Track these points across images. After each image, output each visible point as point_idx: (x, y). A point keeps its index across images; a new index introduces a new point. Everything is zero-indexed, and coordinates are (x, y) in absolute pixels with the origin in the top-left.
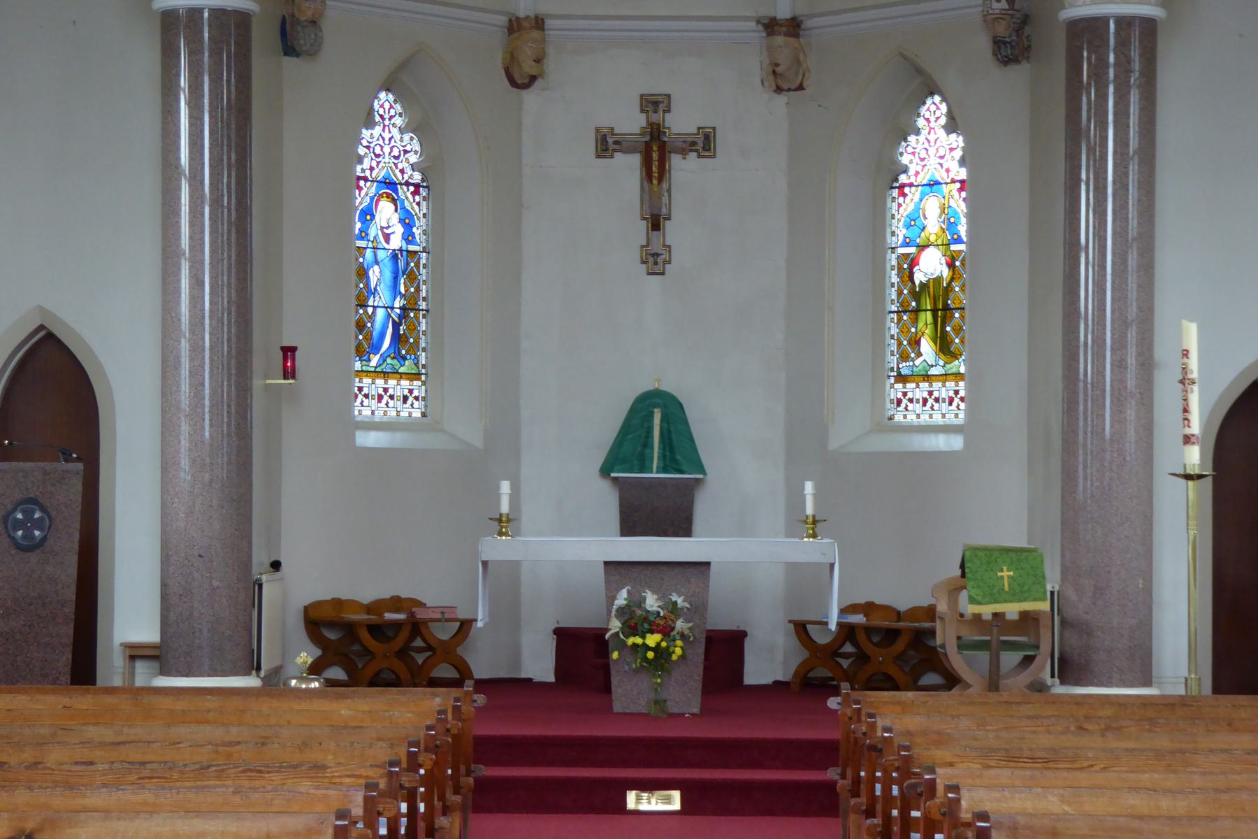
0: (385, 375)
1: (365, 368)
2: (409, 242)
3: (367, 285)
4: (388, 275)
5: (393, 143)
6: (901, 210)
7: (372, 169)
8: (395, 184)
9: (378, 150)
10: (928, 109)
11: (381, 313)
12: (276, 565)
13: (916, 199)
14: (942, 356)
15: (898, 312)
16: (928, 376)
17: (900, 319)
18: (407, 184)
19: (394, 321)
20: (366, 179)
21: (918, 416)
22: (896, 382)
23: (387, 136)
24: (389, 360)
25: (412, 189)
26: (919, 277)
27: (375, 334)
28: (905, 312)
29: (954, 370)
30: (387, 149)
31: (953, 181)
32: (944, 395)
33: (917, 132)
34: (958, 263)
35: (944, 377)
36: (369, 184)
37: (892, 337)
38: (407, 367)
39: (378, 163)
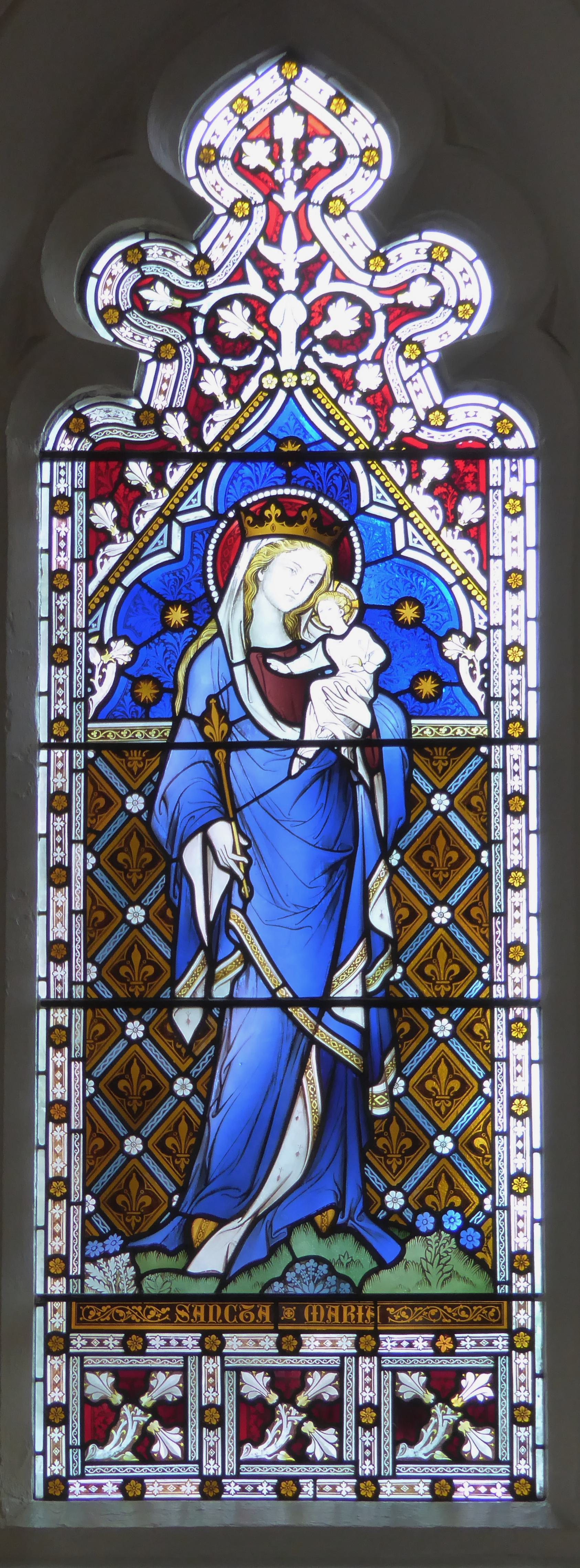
0: (284, 1313)
1: (153, 1285)
2: (411, 703)
3: (173, 908)
4: (296, 860)
5: (324, 284)
7: (199, 407)
8: (339, 456)
9: (236, 323)
11: (250, 1036)
12: (297, 1154)
17: (96, 1043)
18: (411, 452)
19: (331, 1064)
20: (162, 454)
23: (288, 256)
24: (305, 1243)
25: (436, 469)
27: (221, 1128)
30: (288, 315)
36: (175, 475)
38: (423, 1265)
39: (236, 382)
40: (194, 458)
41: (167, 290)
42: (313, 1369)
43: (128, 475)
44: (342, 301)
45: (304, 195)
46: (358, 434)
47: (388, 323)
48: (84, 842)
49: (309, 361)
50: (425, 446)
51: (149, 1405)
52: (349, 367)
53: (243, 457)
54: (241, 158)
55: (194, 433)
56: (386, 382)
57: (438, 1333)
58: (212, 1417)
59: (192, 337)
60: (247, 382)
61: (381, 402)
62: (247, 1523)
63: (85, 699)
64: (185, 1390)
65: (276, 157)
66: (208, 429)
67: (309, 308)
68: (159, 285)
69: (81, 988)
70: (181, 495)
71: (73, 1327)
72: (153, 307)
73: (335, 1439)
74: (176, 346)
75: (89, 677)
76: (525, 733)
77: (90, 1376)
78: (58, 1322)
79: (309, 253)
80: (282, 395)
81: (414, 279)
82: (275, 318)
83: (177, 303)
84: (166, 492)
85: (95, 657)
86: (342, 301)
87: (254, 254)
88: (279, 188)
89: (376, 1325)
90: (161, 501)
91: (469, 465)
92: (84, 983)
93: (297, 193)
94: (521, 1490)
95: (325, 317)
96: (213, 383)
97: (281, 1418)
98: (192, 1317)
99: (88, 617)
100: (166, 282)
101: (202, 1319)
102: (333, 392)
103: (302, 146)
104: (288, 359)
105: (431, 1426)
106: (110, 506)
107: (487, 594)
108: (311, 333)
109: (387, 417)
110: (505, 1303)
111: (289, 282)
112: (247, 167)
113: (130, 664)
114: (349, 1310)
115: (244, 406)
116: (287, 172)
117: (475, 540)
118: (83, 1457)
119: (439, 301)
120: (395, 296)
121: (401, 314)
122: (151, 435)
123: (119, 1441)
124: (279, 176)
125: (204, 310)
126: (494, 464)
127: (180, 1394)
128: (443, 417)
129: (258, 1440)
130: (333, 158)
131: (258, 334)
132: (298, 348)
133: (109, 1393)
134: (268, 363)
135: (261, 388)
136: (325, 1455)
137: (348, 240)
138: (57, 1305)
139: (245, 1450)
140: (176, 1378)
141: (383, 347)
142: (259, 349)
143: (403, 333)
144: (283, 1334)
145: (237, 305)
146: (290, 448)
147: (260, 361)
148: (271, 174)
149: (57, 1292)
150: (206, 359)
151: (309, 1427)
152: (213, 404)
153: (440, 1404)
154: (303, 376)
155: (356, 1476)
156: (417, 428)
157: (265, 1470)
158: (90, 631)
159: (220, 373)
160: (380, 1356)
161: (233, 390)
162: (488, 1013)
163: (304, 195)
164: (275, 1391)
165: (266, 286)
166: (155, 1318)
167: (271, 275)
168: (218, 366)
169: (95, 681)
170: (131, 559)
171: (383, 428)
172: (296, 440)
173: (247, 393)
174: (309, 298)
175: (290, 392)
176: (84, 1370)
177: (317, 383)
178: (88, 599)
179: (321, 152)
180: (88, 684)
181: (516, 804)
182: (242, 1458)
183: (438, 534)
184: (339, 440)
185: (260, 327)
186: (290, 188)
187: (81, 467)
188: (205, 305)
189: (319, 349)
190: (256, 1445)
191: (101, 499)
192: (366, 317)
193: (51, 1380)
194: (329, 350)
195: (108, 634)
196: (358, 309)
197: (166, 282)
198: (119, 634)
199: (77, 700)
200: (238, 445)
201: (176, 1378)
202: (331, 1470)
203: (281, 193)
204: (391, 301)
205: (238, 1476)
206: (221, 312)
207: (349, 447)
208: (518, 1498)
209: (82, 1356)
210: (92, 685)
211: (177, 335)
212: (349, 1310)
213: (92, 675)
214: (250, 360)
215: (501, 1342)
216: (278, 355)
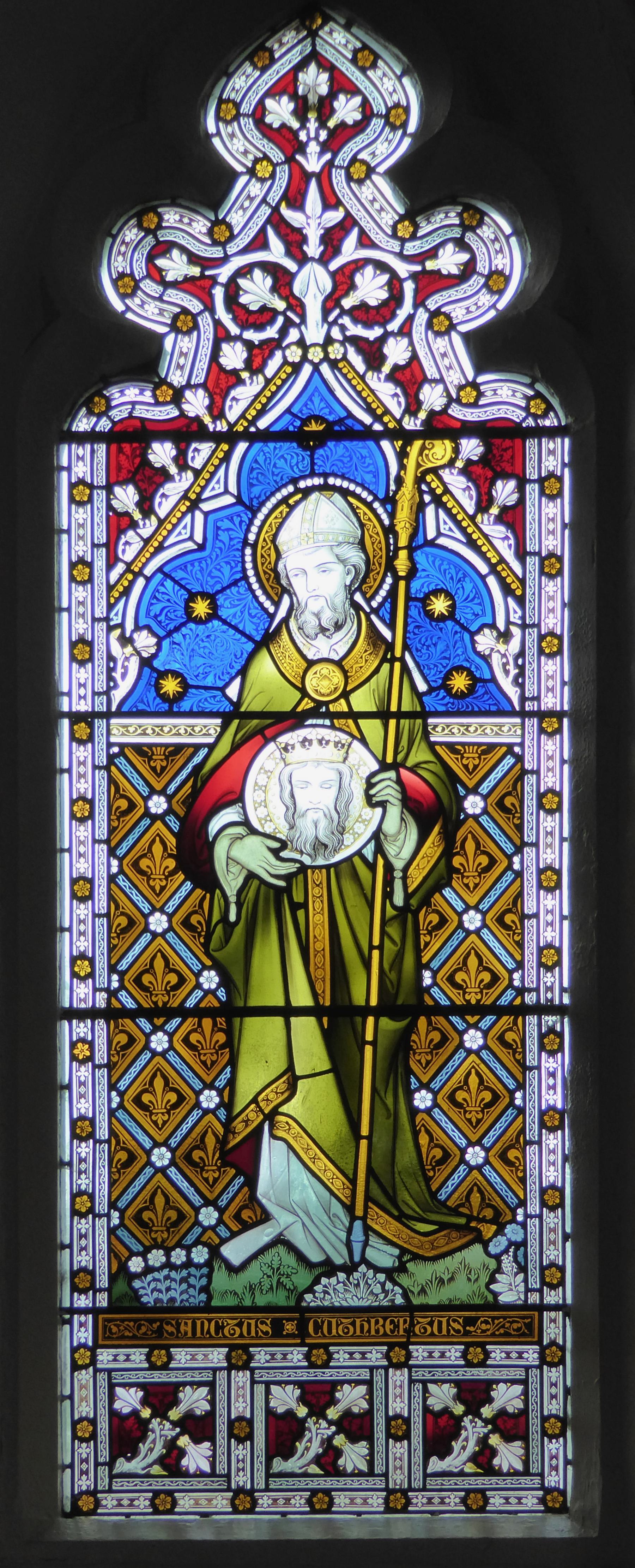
5: (349, 251)
6: (130, 546)
7: (221, 382)
9: (257, 291)
10: (286, 86)
13: (219, 497)
14: (381, 1221)
15: (111, 1014)
16: (302, 1313)
17: (122, 1052)
21: (244, 1499)
22: (105, 1337)
23: (312, 219)
25: (471, 448)
26: (239, 857)
28: (159, 1014)
29: (461, 1290)
30: (313, 283)
31: (439, 427)
32: (240, 1398)
33: (209, 185)
34: (473, 804)
35: (400, 1326)
37: (83, 1130)
39: (256, 357)
40: (217, 438)
41: (185, 258)
42: (498, 1382)
43: (151, 457)
44: (369, 270)
45: (328, 156)
46: (387, 412)
47: (417, 291)
48: (107, 842)
49: (336, 333)
50: (458, 425)
51: (336, 1417)
52: (377, 339)
53: (266, 436)
54: (263, 115)
55: (217, 411)
56: (414, 357)
57: (152, 1348)
58: (399, 1428)
59: (210, 307)
60: (271, 355)
61: (410, 378)
62: (283, 1538)
63: (107, 693)
64: (371, 1402)
65: (301, 113)
66: (231, 407)
67: (333, 275)
68: (175, 253)
69: (104, 995)
70: (207, 476)
71: (100, 1342)
72: (170, 278)
73: (522, 1451)
74: (194, 317)
75: (110, 671)
76: (72, 725)
77: (119, 1391)
78: (85, 1335)
79: (335, 217)
80: (307, 369)
81: (443, 244)
82: (297, 288)
83: (196, 271)
84: (190, 475)
85: (116, 649)
86: (369, 270)
87: (276, 220)
88: (301, 148)
89: (408, 1338)
90: (185, 485)
91: (503, 445)
92: (107, 990)
93: (322, 153)
94: (553, 1502)
95: (352, 287)
96: (233, 357)
97: (310, 1431)
98: (178, 1331)
99: (110, 607)
100: (183, 249)
101: (190, 1334)
102: (361, 367)
103: (327, 102)
104: (314, 332)
105: (305, 1439)
106: (131, 489)
107: (523, 581)
108: (337, 304)
109: (417, 395)
110: (536, 1313)
111: (313, 248)
112: (270, 126)
113: (154, 656)
114: (377, 1322)
115: (268, 381)
116: (311, 131)
117: (510, 525)
118: (110, 1471)
119: (468, 270)
120: (422, 263)
121: (430, 283)
122: (172, 412)
123: (303, 1455)
124: (303, 136)
125: (223, 279)
126: (531, 445)
127: (521, 1406)
128: (474, 393)
129: (288, 1453)
130: (358, 117)
131: (280, 305)
132: (325, 319)
133: (293, 1405)
134: (293, 335)
135: (285, 362)
136: (355, 1467)
137: (378, 203)
138: (553, 1314)
139: (117, 1465)
140: (204, 1391)
141: (410, 318)
142: (280, 320)
143: (432, 303)
144: (312, 1347)
145: (257, 273)
146: (314, 427)
147: (283, 332)
148: (295, 134)
149: (83, 1305)
150: (227, 331)
151: (339, 1441)
152: (234, 378)
153: (158, 1420)
154: (330, 349)
155: (542, 1487)
156: (447, 406)
157: (302, 1483)
158: (112, 623)
159: (239, 346)
160: (410, 1368)
161: (254, 365)
162: (520, 1019)
163: (328, 156)
164: (462, 1403)
165: (289, 253)
166: (145, 1334)
167: (294, 241)
168: (238, 338)
169: (117, 675)
170: (153, 545)
171: (413, 406)
172: (318, 419)
173: (271, 368)
174: (334, 265)
175: (316, 367)
176: (112, 1387)
177: (344, 358)
178: (110, 588)
179: (346, 110)
180: (110, 678)
181: (550, 802)
182: (114, 1472)
183: (472, 518)
184: (367, 419)
185: (281, 297)
186: (313, 148)
187: (101, 449)
188: (224, 273)
189: (346, 320)
190: (442, 1458)
191: (123, 482)
192: (395, 284)
193: (82, 1396)
194: (356, 321)
195: (130, 625)
196: (385, 277)
197: (183, 249)
198: (141, 624)
199: (99, 694)
200: (262, 424)
201: (362, 1389)
202: (364, 1483)
203: (304, 153)
204: (418, 268)
205: (424, 1489)
206: (241, 282)
207: (377, 427)
208: (549, 1510)
209: (109, 1371)
210: (113, 679)
211: (195, 306)
212: (377, 1322)
213: (114, 669)
214: (271, 332)
215: (531, 1355)
216: (303, 328)
